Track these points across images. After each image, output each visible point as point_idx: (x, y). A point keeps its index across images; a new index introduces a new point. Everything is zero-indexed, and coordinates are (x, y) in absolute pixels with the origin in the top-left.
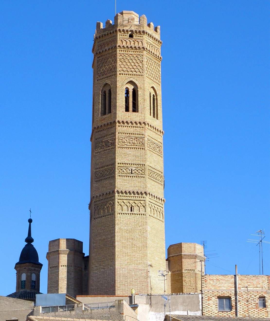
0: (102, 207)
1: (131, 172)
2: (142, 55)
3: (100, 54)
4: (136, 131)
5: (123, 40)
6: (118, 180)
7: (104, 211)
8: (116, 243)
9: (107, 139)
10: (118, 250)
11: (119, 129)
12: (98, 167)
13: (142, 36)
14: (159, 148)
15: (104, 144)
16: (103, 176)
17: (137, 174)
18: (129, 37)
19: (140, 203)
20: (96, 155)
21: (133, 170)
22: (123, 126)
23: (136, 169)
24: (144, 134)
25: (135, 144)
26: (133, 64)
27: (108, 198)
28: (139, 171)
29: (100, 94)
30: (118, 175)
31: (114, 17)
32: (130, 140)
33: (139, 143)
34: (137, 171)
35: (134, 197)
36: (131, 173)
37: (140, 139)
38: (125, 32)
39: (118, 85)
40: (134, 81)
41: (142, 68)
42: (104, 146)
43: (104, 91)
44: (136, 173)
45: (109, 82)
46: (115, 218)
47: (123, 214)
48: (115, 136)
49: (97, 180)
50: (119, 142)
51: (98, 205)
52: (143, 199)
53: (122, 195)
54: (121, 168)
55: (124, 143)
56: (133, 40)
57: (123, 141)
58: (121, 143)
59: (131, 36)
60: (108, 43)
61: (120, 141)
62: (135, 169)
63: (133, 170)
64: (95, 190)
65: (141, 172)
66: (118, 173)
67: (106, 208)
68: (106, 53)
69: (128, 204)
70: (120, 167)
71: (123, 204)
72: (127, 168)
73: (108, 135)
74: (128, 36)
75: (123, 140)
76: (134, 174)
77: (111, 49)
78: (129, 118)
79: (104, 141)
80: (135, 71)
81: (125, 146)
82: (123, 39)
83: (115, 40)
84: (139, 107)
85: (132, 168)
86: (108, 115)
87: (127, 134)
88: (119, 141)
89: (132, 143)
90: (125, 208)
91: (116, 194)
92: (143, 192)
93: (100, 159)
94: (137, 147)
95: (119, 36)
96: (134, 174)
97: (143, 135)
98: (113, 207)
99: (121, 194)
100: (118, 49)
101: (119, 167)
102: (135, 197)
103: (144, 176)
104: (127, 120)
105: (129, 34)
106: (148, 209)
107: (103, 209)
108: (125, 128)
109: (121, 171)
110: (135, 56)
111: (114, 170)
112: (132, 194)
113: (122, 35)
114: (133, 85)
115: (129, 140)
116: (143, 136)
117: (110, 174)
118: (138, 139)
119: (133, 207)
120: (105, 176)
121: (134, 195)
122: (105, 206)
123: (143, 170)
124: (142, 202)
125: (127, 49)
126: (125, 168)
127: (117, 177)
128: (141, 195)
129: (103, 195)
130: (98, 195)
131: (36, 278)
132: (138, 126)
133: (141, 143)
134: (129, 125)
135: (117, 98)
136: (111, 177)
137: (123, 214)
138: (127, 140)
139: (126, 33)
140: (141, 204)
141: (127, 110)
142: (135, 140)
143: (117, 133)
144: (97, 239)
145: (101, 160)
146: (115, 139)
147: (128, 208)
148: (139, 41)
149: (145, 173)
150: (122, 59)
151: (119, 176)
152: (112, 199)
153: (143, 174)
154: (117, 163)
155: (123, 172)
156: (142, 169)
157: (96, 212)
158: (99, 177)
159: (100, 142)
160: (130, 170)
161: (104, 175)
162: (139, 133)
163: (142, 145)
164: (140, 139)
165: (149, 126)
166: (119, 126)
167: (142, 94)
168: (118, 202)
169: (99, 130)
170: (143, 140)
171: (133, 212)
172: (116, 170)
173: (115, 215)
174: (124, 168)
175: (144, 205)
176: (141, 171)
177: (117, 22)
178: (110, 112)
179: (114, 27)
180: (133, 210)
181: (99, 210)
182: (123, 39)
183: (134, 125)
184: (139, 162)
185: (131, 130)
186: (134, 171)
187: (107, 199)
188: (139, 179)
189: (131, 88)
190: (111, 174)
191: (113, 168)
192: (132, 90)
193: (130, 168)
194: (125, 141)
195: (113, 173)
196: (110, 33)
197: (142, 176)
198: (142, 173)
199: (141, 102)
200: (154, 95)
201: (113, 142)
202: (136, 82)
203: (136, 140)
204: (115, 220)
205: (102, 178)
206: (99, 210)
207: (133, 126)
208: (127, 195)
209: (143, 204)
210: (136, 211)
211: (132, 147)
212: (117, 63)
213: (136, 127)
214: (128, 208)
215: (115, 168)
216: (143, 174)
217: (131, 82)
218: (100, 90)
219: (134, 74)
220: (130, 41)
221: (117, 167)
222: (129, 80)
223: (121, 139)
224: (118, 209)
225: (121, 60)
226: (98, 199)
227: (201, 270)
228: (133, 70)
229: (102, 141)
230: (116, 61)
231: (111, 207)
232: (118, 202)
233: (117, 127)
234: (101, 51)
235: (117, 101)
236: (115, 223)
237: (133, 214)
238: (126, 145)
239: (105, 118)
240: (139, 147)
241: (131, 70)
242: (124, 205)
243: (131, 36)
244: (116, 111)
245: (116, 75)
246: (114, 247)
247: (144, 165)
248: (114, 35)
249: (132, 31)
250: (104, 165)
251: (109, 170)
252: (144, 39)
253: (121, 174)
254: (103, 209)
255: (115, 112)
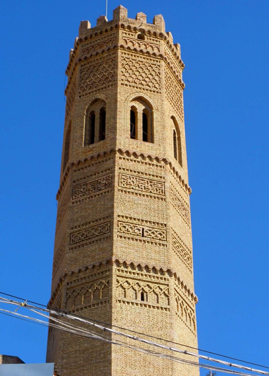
0: (84, 291)
1: (141, 233)
2: (159, 66)
3: (87, 60)
4: (151, 170)
5: (128, 41)
6: (119, 244)
7: (87, 298)
8: (113, 355)
9: (97, 179)
10: (117, 368)
11: (120, 162)
12: (76, 224)
13: (158, 40)
15: (89, 187)
16: (88, 238)
17: (153, 238)
18: (138, 38)
19: (158, 288)
20: (74, 207)
21: (146, 231)
22: (127, 159)
23: (151, 230)
24: (164, 177)
25: (149, 189)
26: (144, 75)
27: (97, 274)
28: (156, 233)
29: (84, 115)
30: (118, 235)
31: (113, 11)
32: (139, 182)
33: (156, 189)
34: (153, 233)
35: (148, 276)
36: (141, 235)
37: (157, 184)
38: (132, 30)
39: (118, 99)
40: (146, 97)
41: (159, 83)
42: (89, 190)
43: (91, 111)
44: (151, 236)
45: (101, 96)
46: (111, 307)
47: (126, 302)
48: (113, 172)
49: (74, 246)
50: (120, 182)
51: (75, 289)
52: (162, 281)
53: (126, 269)
54: (124, 224)
55: (130, 185)
56: (144, 43)
57: (127, 181)
58: (124, 185)
59: (141, 37)
60: (100, 46)
61: (122, 182)
62: (149, 229)
64: (69, 264)
65: (159, 236)
66: (118, 231)
67: (90, 292)
68: (98, 57)
69: (136, 287)
70: (121, 223)
71: (127, 285)
72: (135, 225)
73: (99, 173)
74: (136, 36)
75: (127, 180)
76: (148, 237)
77: (114, 29)
78: (138, 149)
79: (89, 183)
80: (148, 85)
81: (132, 190)
82: (128, 39)
83: (116, 39)
84: (155, 136)
85: (144, 227)
86: (99, 143)
87: (135, 172)
88: (120, 180)
89: (143, 188)
90: (130, 292)
91: (115, 267)
92: (165, 270)
93: (82, 211)
94: (152, 194)
95: (121, 33)
96: (148, 237)
97: (163, 178)
98: (106, 290)
99: (122, 268)
100: (119, 50)
101: (119, 223)
102: (150, 276)
103: (165, 243)
105: (137, 34)
106: (173, 302)
107: (85, 295)
108: (131, 163)
109: (123, 229)
110: (147, 65)
111: (110, 226)
112: (144, 270)
113: (126, 33)
114: (144, 105)
115: (137, 182)
118: (153, 183)
119: (146, 293)
121: (147, 273)
122: (90, 288)
123: (164, 233)
125: (135, 53)
126: (132, 225)
127: (115, 238)
128: (161, 274)
129: (86, 270)
130: (76, 271)
132: (153, 163)
133: (160, 189)
134: (137, 160)
135: (118, 117)
136: (104, 238)
137: (126, 302)
138: (135, 181)
139: (132, 32)
140: (160, 291)
141: (133, 135)
142: (148, 184)
143: (117, 168)
144: (71, 349)
145: (83, 213)
146: (113, 177)
147: (136, 293)
148: (154, 46)
149: (166, 237)
150: (126, 64)
151: (119, 236)
152: (104, 275)
153: (164, 241)
154: (115, 215)
155: (126, 232)
156: (162, 232)
157: (70, 300)
158: (78, 240)
159: (82, 185)
160: (139, 230)
163: (161, 193)
164: (157, 183)
166: (120, 158)
167: (159, 119)
168: (118, 282)
169: (80, 167)
170: (163, 186)
171: (145, 302)
172: (115, 226)
173: (112, 303)
174: (128, 225)
175: (166, 292)
176: (161, 234)
177: (119, 16)
178: (102, 137)
180: (145, 298)
181: (76, 297)
182: (128, 39)
183: (147, 160)
184: (157, 219)
185: (142, 168)
186: (148, 232)
187: (94, 275)
188: (157, 248)
189: (140, 108)
190: (104, 233)
191: (107, 223)
193: (140, 226)
194: (132, 183)
196: (106, 31)
197: (161, 242)
199: (157, 128)
201: (108, 182)
202: (150, 101)
203: (149, 184)
204: (111, 312)
205: (85, 242)
206: (76, 297)
207: (145, 161)
208: (134, 271)
209: (164, 290)
210: (151, 299)
211: (144, 193)
212: (117, 68)
213: (150, 164)
214: (136, 293)
215: (112, 223)
216: (164, 241)
217: (140, 99)
218: (85, 109)
219: (145, 88)
220: (139, 44)
221: (115, 221)
222: (137, 95)
223: (124, 179)
224: (116, 292)
225: (124, 65)
226: (74, 278)
228: (144, 83)
229: (87, 184)
230: (115, 66)
231: (102, 289)
232: (118, 282)
233: (117, 159)
234: (88, 56)
235: (118, 121)
236: (111, 316)
237: (145, 305)
238: (133, 188)
239: (92, 148)
240: (156, 196)
241: (140, 82)
242: (128, 288)
243: (141, 37)
244: (115, 135)
245: (115, 85)
246: (110, 362)
248: (112, 32)
249: (143, 31)
250: (88, 220)
251: (100, 227)
252: (162, 45)
253: (123, 235)
254: (85, 295)
255: (114, 136)
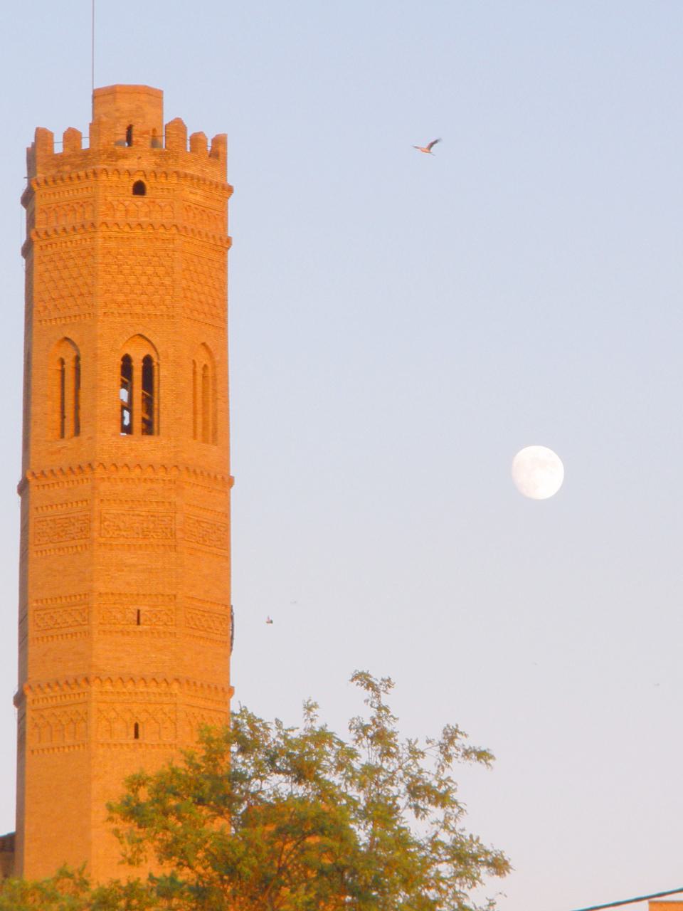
124: (166, 709)
131: (225, 291)
175: (173, 717)
179: (90, 157)
192: (142, 364)
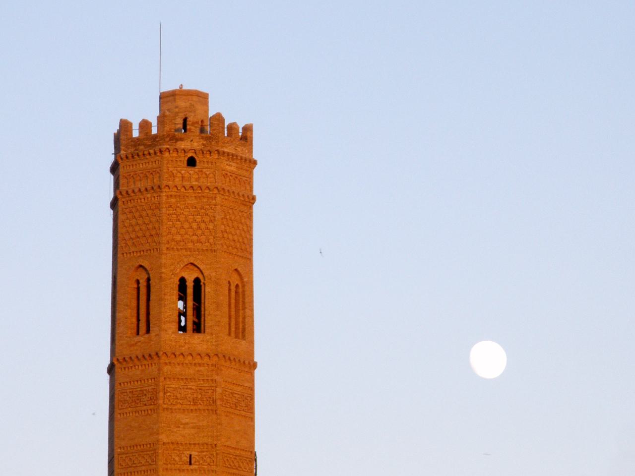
14: (246, 401)
63: (192, 456)
81: (179, 406)
104: (183, 350)
116: (214, 383)
117: (148, 465)
120: (137, 466)
132: (203, 362)
161: (135, 464)
162: (205, 378)
165: (226, 361)
166: (166, 364)
195: (154, 463)
198: (211, 462)
200: (237, 286)
222: (186, 261)
227: (171, 96)
247: (216, 445)
